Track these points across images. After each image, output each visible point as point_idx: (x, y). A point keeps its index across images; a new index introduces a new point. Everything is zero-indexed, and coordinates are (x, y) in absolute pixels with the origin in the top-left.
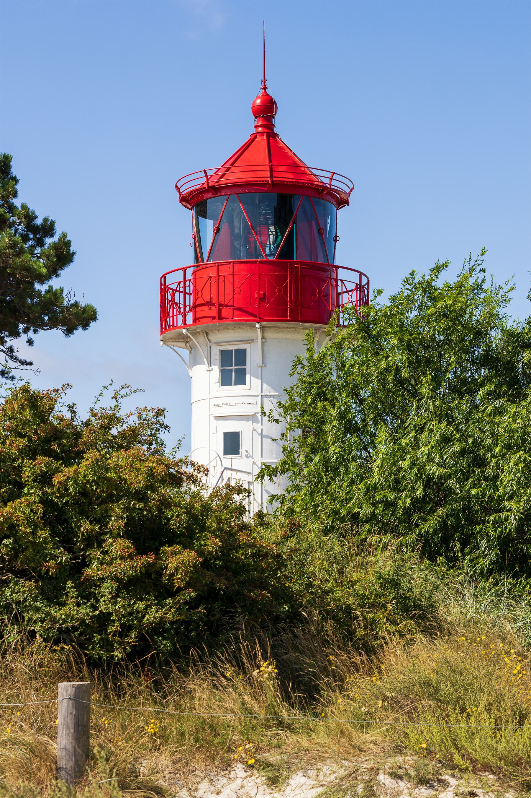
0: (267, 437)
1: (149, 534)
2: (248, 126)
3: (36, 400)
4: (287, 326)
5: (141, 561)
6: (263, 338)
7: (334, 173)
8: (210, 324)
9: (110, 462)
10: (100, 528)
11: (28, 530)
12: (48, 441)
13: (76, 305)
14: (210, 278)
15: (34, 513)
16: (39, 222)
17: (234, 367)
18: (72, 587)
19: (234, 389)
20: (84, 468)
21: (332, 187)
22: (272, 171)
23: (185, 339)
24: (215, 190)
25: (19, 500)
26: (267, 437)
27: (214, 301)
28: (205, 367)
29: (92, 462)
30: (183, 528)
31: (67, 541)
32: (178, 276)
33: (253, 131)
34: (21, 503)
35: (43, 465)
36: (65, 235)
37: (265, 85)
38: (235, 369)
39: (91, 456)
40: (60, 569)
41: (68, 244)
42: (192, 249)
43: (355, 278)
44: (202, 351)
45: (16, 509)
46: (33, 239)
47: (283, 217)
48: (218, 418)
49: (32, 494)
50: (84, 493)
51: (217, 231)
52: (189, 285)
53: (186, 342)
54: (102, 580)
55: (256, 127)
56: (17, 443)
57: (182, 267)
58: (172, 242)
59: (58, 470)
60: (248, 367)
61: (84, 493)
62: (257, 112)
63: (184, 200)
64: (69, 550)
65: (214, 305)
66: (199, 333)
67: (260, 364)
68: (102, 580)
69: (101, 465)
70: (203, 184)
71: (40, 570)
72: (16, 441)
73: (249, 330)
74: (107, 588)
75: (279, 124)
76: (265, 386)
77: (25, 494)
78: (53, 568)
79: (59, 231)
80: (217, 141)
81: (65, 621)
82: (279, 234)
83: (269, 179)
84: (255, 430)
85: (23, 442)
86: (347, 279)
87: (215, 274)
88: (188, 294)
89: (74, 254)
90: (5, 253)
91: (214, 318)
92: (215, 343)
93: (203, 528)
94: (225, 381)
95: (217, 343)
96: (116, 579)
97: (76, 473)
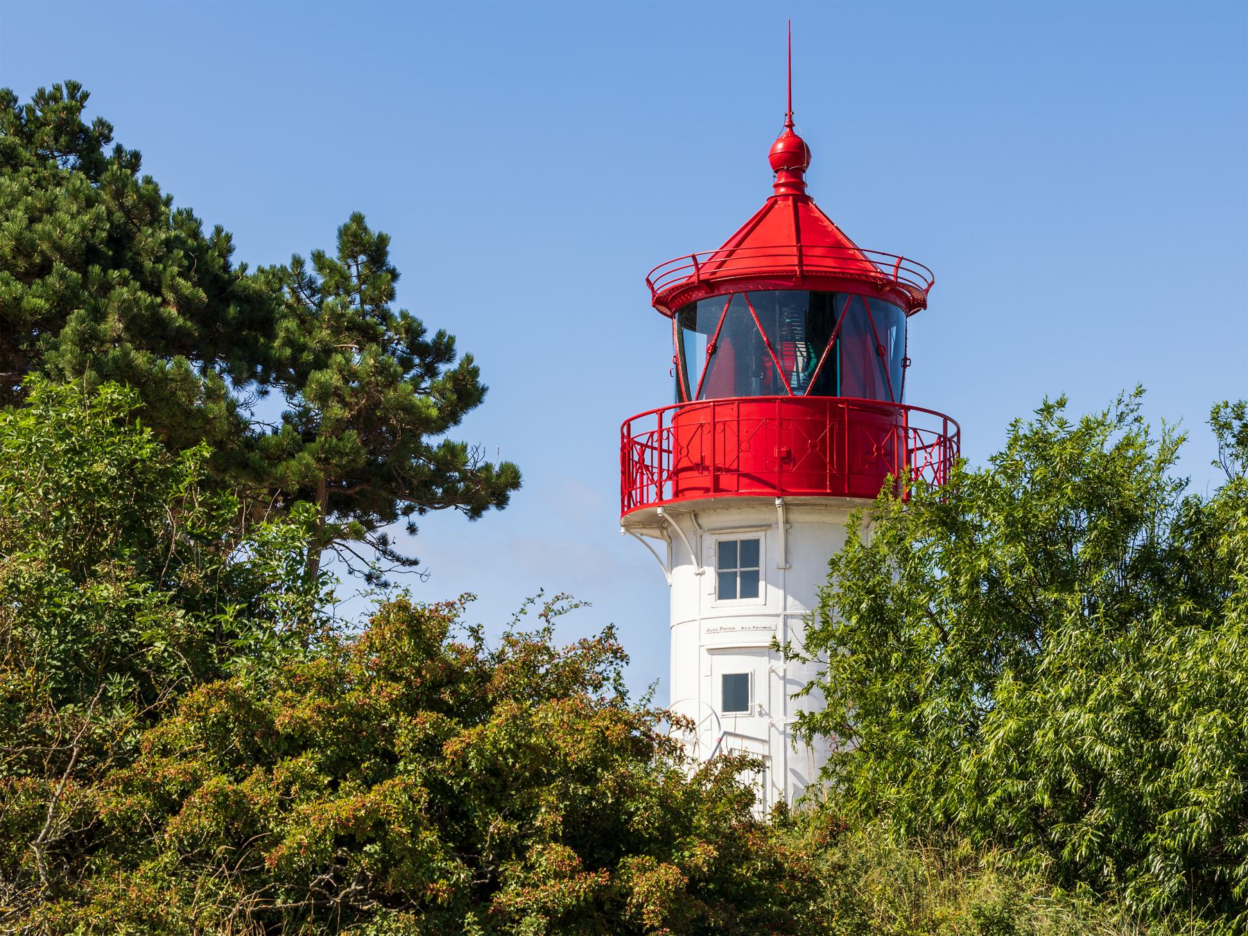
1: (601, 837)
2: (762, 186)
3: (419, 623)
6: (787, 522)
7: (902, 258)
9: (535, 719)
10: (520, 827)
11: (404, 831)
12: (436, 686)
13: (488, 467)
14: (701, 426)
16: (429, 338)
17: (739, 570)
19: (740, 605)
22: (801, 256)
23: (660, 524)
24: (709, 286)
25: (390, 781)
27: (708, 462)
28: (693, 568)
30: (654, 828)
31: (466, 849)
32: (651, 423)
33: (772, 193)
34: (394, 786)
35: (428, 725)
36: (469, 359)
39: (505, 709)
40: (455, 894)
41: (475, 372)
42: (673, 381)
43: (936, 425)
44: (687, 543)
48: (712, 651)
49: (411, 773)
50: (494, 770)
51: (713, 351)
53: (662, 528)
54: (523, 912)
55: (777, 186)
56: (389, 690)
59: (451, 733)
60: (762, 568)
61: (494, 770)
62: (778, 163)
64: (471, 863)
65: (707, 469)
66: (683, 514)
67: (782, 564)
68: (523, 912)
69: (520, 723)
71: (423, 895)
73: (764, 509)
75: (816, 182)
76: (790, 599)
79: (460, 352)
80: (712, 209)
85: (397, 689)
86: (924, 427)
87: (709, 419)
91: (707, 490)
93: (687, 830)
94: (725, 591)
95: (713, 531)
96: (544, 910)
97: (482, 737)
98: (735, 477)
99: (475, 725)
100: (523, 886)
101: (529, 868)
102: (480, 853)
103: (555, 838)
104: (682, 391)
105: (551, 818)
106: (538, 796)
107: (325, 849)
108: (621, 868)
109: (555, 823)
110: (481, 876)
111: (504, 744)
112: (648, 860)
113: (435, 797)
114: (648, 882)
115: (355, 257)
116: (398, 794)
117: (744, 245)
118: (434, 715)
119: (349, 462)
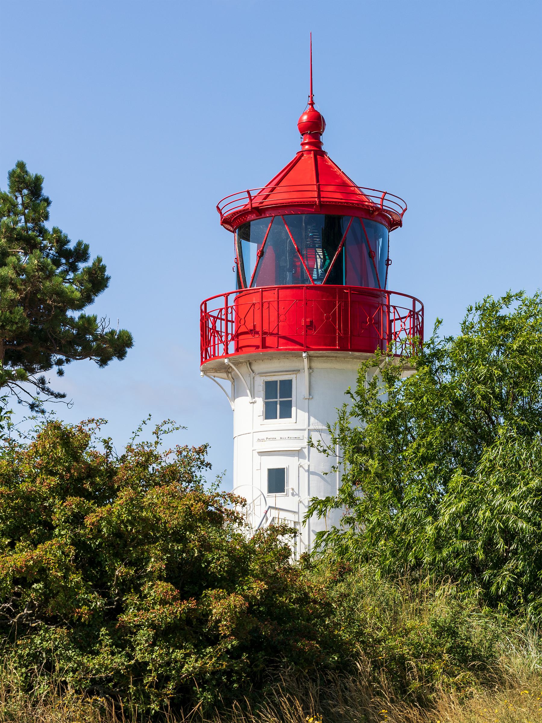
0: (314, 473)
2: (294, 144)
3: (68, 436)
4: (335, 355)
5: (180, 608)
6: (310, 368)
7: (386, 193)
8: (252, 353)
11: (59, 574)
12: (80, 480)
13: (112, 333)
14: (254, 304)
15: (65, 556)
16: (71, 246)
17: (278, 400)
18: (106, 634)
19: (279, 423)
20: (118, 506)
21: (384, 208)
22: (319, 191)
23: (226, 369)
24: (259, 211)
25: (49, 542)
26: (314, 473)
27: (258, 329)
28: (249, 399)
29: (126, 501)
30: (224, 571)
31: (101, 586)
32: (220, 303)
33: (300, 149)
34: (52, 545)
35: (74, 506)
36: (99, 260)
37: (312, 101)
38: (280, 401)
39: (125, 494)
41: (103, 269)
42: (235, 274)
43: (408, 303)
44: (244, 382)
45: (46, 552)
46: (66, 264)
47: (331, 239)
48: (261, 453)
49: (63, 536)
50: (118, 534)
51: (261, 254)
52: (232, 312)
53: (228, 372)
54: (138, 627)
55: (303, 144)
56: (48, 481)
57: (224, 293)
58: (214, 268)
59: (89, 510)
60: (294, 399)
61: (118, 534)
62: (304, 129)
63: (226, 222)
65: (257, 333)
66: (241, 363)
67: (307, 396)
68: (138, 627)
69: (135, 504)
70: (246, 205)
71: (72, 617)
72: (47, 479)
73: (295, 359)
74: (143, 636)
76: (312, 419)
77: (56, 536)
78: (86, 614)
80: (261, 159)
81: (98, 671)
82: (327, 257)
83: (316, 199)
84: (301, 466)
85: (54, 481)
86: (400, 305)
87: (259, 300)
88: (230, 321)
89: (108, 279)
90: (34, 276)
91: (257, 347)
92: (259, 374)
93: (245, 572)
94: (270, 414)
95: (261, 374)
96: (153, 626)
97: (110, 513)
98: (276, 339)
99: (105, 505)
100: (139, 610)
101: (143, 597)
102: (109, 588)
103: (160, 578)
104: (241, 281)
105: (157, 566)
106: (148, 551)
107: (7, 586)
108: (204, 597)
109: (161, 569)
110: (110, 603)
111: (124, 517)
112: (221, 592)
113: (79, 552)
114: (222, 606)
115: (20, 192)
116: (52, 551)
117: (281, 184)
118: (78, 499)
119: (18, 328)
